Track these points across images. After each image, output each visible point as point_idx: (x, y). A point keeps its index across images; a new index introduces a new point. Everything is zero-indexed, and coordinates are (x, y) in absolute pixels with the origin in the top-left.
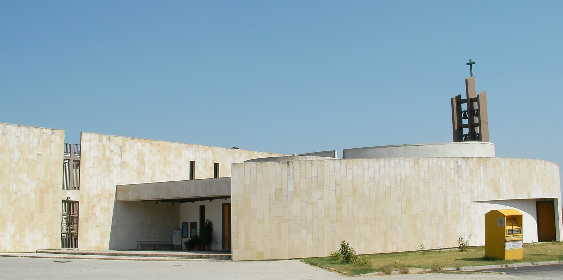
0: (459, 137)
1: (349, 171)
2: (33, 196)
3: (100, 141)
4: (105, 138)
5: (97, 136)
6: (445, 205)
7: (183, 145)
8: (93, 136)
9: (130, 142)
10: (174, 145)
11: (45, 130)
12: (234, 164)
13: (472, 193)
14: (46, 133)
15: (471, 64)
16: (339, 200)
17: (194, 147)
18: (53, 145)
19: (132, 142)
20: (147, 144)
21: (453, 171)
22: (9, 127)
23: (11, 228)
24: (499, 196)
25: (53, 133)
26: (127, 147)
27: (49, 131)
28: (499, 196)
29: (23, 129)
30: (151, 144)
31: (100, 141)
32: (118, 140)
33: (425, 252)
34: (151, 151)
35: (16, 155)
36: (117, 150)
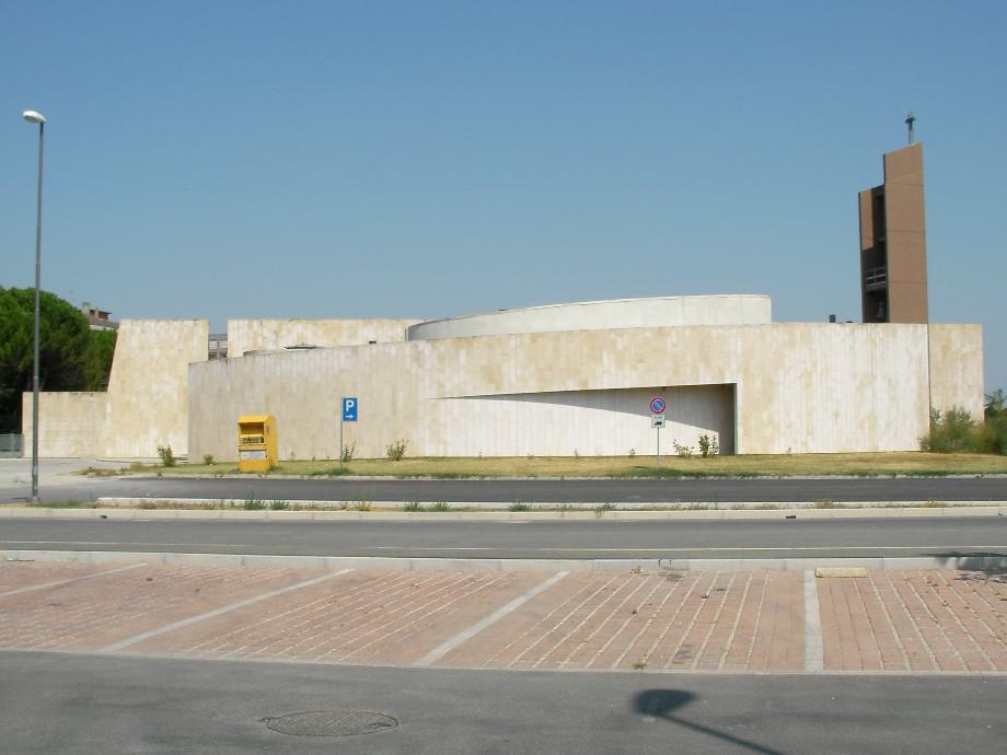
0: (210, 335)
1: (278, 367)
2: (175, 396)
3: (250, 327)
4: (256, 324)
5: (246, 322)
6: (394, 404)
7: (360, 322)
8: (241, 323)
9: (287, 325)
10: (346, 323)
11: (186, 322)
12: (190, 364)
13: (441, 386)
14: (187, 326)
15: (910, 121)
16: (267, 400)
17: (375, 323)
18: (195, 337)
19: (290, 325)
20: (310, 326)
21: (408, 360)
22: (147, 323)
23: (154, 432)
24: (498, 388)
25: (196, 325)
26: (284, 332)
27: (191, 323)
28: (723, 379)
29: (162, 323)
30: (315, 325)
31: (250, 327)
32: (273, 324)
33: (577, 458)
34: (315, 334)
35: (157, 352)
36: (271, 337)
